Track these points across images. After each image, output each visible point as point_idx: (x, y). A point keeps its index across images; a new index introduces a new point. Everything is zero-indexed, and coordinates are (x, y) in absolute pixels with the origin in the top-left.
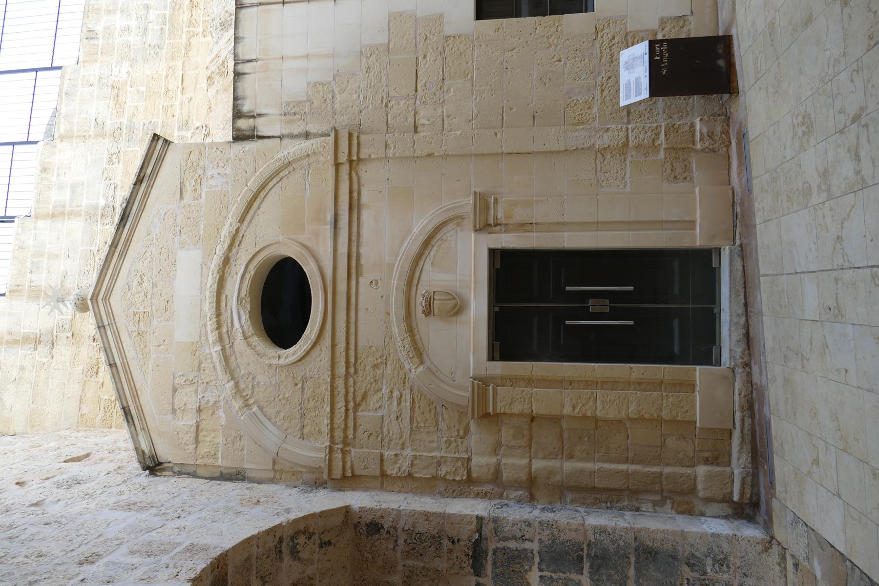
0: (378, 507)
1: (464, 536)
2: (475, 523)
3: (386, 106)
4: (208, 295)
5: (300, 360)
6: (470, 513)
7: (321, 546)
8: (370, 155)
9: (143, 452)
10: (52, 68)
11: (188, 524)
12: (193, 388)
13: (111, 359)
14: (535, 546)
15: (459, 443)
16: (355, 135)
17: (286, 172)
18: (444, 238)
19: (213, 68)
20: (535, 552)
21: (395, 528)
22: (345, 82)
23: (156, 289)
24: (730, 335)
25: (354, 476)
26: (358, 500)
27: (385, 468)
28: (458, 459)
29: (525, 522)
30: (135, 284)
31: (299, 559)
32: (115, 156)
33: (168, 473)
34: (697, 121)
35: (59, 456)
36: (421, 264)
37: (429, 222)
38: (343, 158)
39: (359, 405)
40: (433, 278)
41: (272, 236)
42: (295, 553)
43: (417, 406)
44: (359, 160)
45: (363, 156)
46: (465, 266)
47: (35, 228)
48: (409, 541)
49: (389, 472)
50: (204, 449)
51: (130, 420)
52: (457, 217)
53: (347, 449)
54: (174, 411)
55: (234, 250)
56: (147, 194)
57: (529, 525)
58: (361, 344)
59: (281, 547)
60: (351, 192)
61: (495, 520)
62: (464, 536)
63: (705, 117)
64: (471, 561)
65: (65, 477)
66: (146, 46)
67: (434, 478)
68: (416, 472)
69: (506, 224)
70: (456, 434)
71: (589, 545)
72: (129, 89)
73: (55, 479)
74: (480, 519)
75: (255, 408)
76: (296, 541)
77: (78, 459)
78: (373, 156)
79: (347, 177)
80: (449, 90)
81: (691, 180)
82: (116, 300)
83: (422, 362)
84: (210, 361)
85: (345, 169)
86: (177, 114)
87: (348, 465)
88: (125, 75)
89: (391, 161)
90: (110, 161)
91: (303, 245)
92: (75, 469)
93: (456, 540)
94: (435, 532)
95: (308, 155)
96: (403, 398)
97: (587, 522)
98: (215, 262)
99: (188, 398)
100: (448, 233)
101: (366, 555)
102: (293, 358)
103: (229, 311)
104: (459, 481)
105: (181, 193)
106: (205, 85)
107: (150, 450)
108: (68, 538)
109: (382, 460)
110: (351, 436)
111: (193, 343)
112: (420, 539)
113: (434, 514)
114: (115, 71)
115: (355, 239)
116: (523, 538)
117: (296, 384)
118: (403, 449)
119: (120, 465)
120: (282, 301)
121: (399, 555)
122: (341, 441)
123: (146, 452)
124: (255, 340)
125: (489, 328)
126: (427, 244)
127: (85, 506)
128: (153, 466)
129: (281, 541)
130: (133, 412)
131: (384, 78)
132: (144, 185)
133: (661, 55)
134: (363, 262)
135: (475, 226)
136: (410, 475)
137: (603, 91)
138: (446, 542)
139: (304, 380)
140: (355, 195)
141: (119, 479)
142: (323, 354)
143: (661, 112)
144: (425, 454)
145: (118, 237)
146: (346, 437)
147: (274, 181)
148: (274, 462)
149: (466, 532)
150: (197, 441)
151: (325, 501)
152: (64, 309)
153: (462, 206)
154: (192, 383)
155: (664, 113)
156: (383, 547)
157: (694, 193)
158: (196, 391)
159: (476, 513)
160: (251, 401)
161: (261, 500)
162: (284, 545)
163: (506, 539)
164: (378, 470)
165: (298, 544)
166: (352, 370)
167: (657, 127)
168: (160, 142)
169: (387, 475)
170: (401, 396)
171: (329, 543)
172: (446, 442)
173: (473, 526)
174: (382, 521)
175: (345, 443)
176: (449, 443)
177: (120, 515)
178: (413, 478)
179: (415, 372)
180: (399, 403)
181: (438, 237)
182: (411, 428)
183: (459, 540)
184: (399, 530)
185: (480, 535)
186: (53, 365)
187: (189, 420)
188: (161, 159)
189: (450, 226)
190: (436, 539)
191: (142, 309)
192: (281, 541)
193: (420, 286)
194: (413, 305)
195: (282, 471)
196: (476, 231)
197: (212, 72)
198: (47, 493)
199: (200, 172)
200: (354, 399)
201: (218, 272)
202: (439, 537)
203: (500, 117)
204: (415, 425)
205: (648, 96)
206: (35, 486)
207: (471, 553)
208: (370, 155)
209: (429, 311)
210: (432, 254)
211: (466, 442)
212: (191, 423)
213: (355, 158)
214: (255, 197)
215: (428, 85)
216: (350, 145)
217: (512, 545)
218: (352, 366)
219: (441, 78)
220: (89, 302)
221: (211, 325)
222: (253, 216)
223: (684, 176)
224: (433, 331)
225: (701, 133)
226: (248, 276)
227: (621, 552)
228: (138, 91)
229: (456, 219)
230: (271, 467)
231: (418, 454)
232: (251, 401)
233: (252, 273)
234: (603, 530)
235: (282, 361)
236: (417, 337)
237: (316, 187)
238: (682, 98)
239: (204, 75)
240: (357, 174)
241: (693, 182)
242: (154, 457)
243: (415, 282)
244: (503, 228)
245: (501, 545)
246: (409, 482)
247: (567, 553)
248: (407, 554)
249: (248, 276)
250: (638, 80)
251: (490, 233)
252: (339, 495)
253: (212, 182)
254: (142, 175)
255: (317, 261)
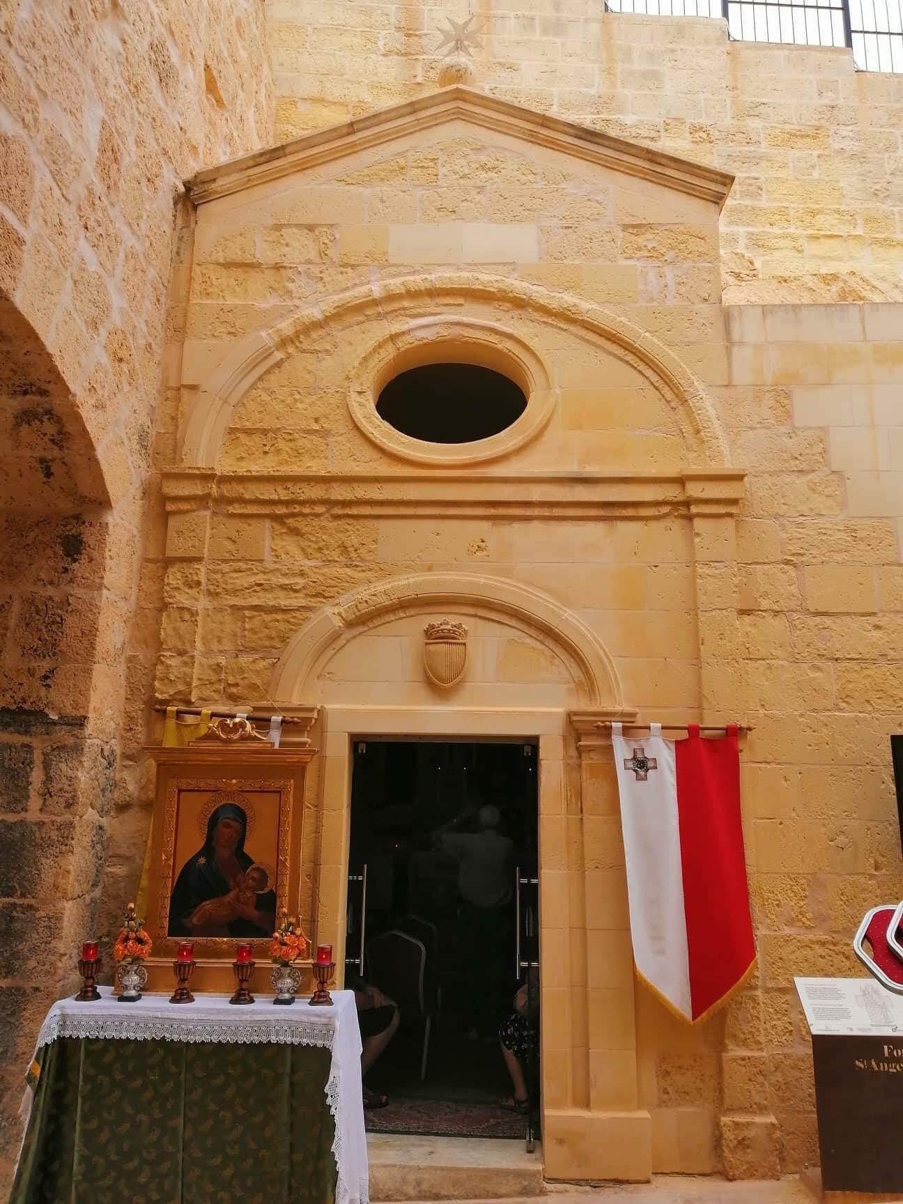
0: (107, 554)
1: (55, 696)
2: (75, 713)
3: (787, 562)
4: (465, 274)
5: (357, 427)
6: (91, 706)
7: (42, 461)
8: (698, 535)
9: (214, 180)
10: (848, 32)
11: (71, 240)
12: (313, 255)
13: (361, 125)
14: (33, 813)
15: (217, 686)
16: (733, 510)
17: (669, 395)
18: (557, 661)
19: (852, 281)
20: (23, 814)
21: (71, 581)
22: (828, 491)
23: (474, 193)
24: (385, 1166)
25: (166, 516)
26: (123, 524)
27: (178, 565)
28: (189, 684)
29: (74, 797)
30: (483, 158)
31: (18, 425)
32: (704, 135)
33: (179, 221)
34: (772, 1119)
35: (219, 59)
36: (513, 622)
37: (583, 636)
38: (694, 490)
39: (283, 523)
40: (486, 643)
41: (558, 374)
42: (27, 416)
43: (279, 617)
44: (690, 518)
45: (698, 523)
46: (499, 700)
47: (586, 21)
48: (50, 604)
49: (170, 570)
50: (223, 279)
51: (262, 159)
52: (592, 684)
53: (211, 504)
54: (278, 227)
55: (536, 315)
56: (631, 171)
57: (69, 806)
58: (382, 524)
59: (33, 393)
60: (635, 505)
61: (78, 749)
62: (55, 696)
63: (778, 1134)
64: (14, 707)
65: (175, 59)
66: (888, 178)
67: (159, 645)
68: (169, 616)
69: (580, 766)
70: (231, 680)
71: (30, 907)
72: (816, 153)
73: (169, 44)
74: (81, 722)
75: (279, 355)
76: (45, 418)
77: (211, 86)
78: (697, 540)
79: (660, 498)
80: (818, 669)
81: (662, 1103)
82: (458, 130)
83: (350, 625)
84: (357, 281)
85: (671, 493)
86: (776, 230)
87: (185, 506)
88: (837, 146)
89: (688, 571)
90: (695, 129)
91: (546, 427)
92: (191, 77)
93: (48, 682)
94: (62, 646)
95: (698, 432)
96: (293, 595)
97: (68, 905)
98: (518, 285)
99: (299, 248)
100: (561, 670)
101: (32, 535)
102: (359, 415)
103: (438, 310)
104: (152, 686)
105: (634, 226)
106: (824, 271)
107: (215, 192)
108: (39, 41)
109: (190, 560)
110: (231, 509)
111: (385, 253)
112: (53, 623)
113: (92, 646)
114: (844, 131)
115: (553, 512)
116: (46, 794)
117: (317, 420)
118: (209, 593)
119: (201, 149)
120: (453, 396)
121: (31, 588)
122: (225, 496)
123: (213, 186)
124: (389, 353)
125: (406, 736)
126: (547, 632)
127: (113, 81)
128: (191, 198)
129: (43, 393)
130: (276, 163)
131: (838, 557)
132: (646, 165)
133: (892, 1059)
134: (516, 526)
135: (576, 714)
136: (164, 607)
137: (823, 944)
138: (45, 665)
139: (324, 433)
140: (630, 512)
141: (171, 145)
142: (343, 457)
143: (786, 1051)
144: (199, 630)
145: (561, 128)
146: (230, 501)
147: (654, 378)
148: (193, 388)
149: (58, 701)
150: (228, 265)
151: (122, 470)
152: (445, 50)
153: (611, 692)
154: (322, 254)
155: (785, 1056)
156: (43, 562)
157: (639, 1107)
158: (309, 262)
159: (91, 715)
160: (291, 350)
161: (124, 366)
162: (37, 398)
163: (47, 766)
164: (174, 554)
165: (42, 422)
166: (338, 511)
167: (758, 1043)
168: (719, 188)
169: (165, 568)
170: (296, 591)
171: (49, 474)
172: (218, 665)
173: (69, 710)
174: (84, 559)
175: (222, 500)
176: (218, 668)
177: (93, 132)
178: (161, 610)
179: (332, 614)
180: (283, 587)
181: (559, 650)
182: (244, 608)
183: (48, 686)
184: (68, 589)
185: (54, 723)
186: (373, 56)
187: (264, 252)
188: (690, 191)
189: (576, 672)
190: (51, 648)
191: (442, 171)
192: (43, 393)
193: (472, 620)
194: (444, 609)
195: (178, 400)
196: (569, 715)
197: (845, 282)
198: (140, 25)
199: (670, 256)
200: (293, 515)
201: (500, 290)
202: (54, 654)
203: (770, 758)
204: (247, 613)
205: (815, 1031)
206: (156, 11)
207: (26, 706)
208: (698, 535)
209: (434, 635)
210: (528, 640)
211: (216, 696)
212: (258, 255)
213: (694, 509)
214: (628, 347)
215: (825, 632)
216: (717, 502)
217: (37, 776)
218: (344, 510)
219: (838, 655)
220: (454, 86)
221: (417, 281)
222: (594, 344)
223: (669, 1090)
224: (398, 645)
225: (748, 1125)
226: (493, 338)
227: (17, 964)
228: (813, 167)
229: (587, 682)
230: (185, 382)
231: (199, 618)
232: (291, 350)
233: (500, 346)
234: (53, 930)
235: (353, 398)
236: (392, 617)
237: (643, 449)
238: (812, 1091)
239: (843, 268)
240: (665, 516)
241: (659, 1106)
242: (206, 198)
243: (481, 612)
244: (573, 761)
245: (38, 757)
246: (156, 607)
247: (20, 869)
248: (30, 602)
249: (493, 338)
250: (843, 1014)
251: (565, 739)
252: (134, 490)
253: (652, 275)
254: (663, 161)
255: (520, 450)
